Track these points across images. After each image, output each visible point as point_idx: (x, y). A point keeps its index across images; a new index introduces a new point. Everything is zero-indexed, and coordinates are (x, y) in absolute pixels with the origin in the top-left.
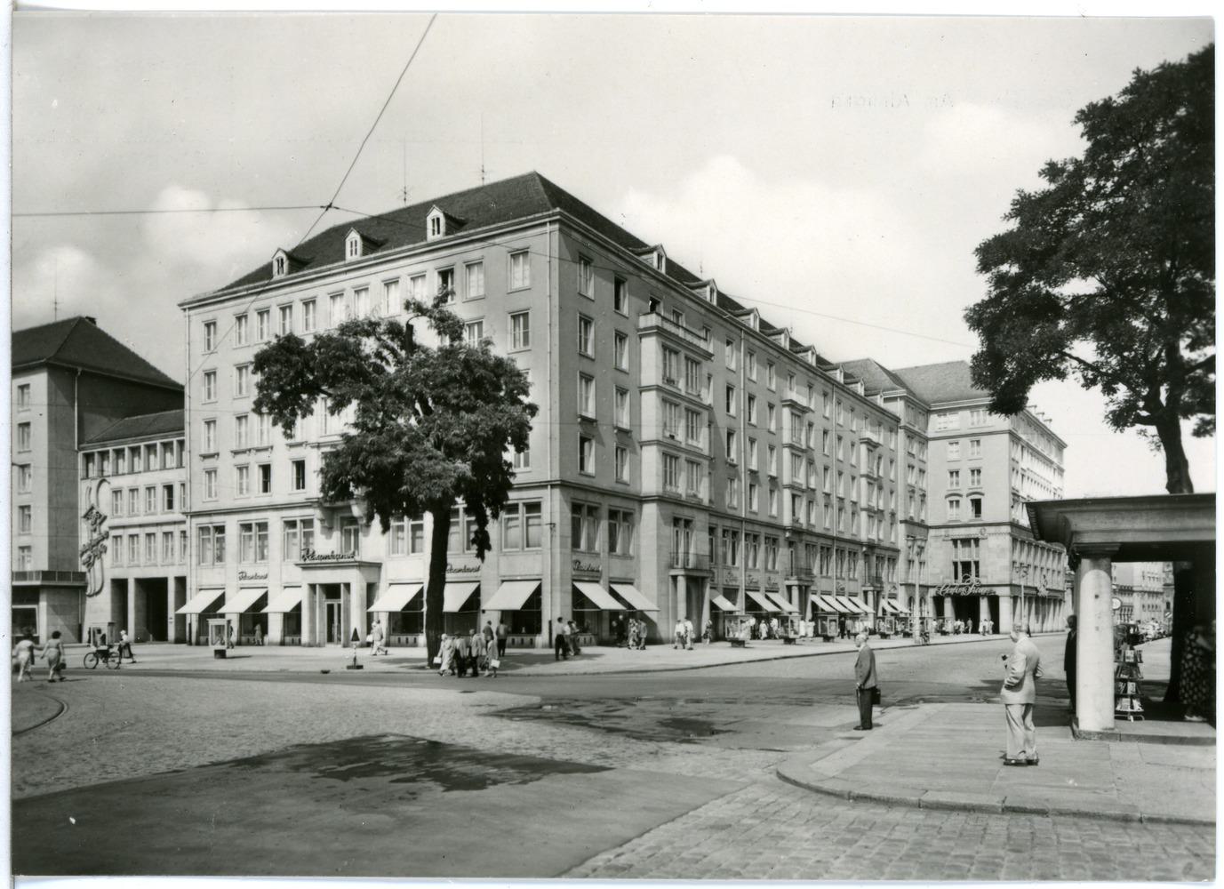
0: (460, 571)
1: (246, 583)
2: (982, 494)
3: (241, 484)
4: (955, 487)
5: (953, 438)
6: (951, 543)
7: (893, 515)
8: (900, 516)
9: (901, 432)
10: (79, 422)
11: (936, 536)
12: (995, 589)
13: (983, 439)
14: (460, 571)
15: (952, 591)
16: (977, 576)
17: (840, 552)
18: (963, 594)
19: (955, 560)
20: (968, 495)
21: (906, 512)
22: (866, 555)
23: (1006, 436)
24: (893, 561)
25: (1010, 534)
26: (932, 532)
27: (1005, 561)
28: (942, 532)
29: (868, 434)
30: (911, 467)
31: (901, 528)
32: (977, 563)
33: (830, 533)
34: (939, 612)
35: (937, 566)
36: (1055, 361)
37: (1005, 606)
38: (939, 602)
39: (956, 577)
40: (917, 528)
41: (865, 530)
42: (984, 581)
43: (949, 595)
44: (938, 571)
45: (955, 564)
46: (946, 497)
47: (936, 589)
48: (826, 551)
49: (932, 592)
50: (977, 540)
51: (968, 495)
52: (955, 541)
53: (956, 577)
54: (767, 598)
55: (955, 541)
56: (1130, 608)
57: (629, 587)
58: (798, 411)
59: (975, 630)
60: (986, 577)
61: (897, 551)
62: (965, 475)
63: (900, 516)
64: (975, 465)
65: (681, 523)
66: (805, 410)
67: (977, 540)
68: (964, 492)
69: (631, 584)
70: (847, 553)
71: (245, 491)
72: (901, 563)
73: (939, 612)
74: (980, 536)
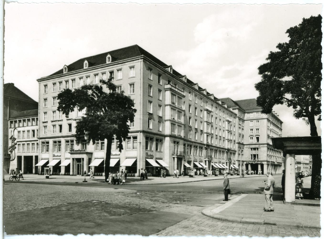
0: (114, 155)
1: (55, 157)
2: (259, 136)
5: (251, 120)
7: (235, 141)
8: (237, 142)
9: (237, 118)
12: (262, 162)
13: (260, 120)
14: (114, 155)
15: (251, 162)
16: (258, 158)
17: (220, 151)
18: (254, 163)
19: (251, 154)
21: (238, 140)
22: (227, 152)
23: (266, 120)
25: (267, 147)
26: (245, 146)
28: (248, 146)
29: (228, 119)
30: (240, 128)
31: (237, 145)
32: (258, 155)
35: (247, 155)
37: (265, 167)
38: (247, 166)
39: (252, 159)
41: (227, 145)
42: (259, 160)
45: (252, 155)
49: (245, 163)
50: (258, 149)
52: (252, 149)
53: (252, 159)
54: (199, 164)
55: (252, 149)
56: (300, 168)
59: (257, 174)
60: (260, 159)
61: (236, 151)
62: (255, 130)
63: (237, 142)
64: (257, 128)
65: (176, 143)
67: (258, 149)
68: (254, 135)
69: (162, 159)
74: (259, 147)
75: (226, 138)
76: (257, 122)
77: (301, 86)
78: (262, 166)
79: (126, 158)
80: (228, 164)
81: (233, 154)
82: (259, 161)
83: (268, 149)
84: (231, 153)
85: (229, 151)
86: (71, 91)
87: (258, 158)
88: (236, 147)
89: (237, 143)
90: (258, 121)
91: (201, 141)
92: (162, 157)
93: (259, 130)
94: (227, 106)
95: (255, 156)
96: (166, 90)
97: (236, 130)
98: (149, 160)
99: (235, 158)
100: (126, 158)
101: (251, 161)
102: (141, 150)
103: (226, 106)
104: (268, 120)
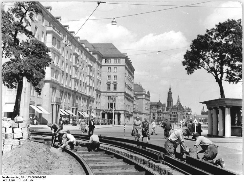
2: (117, 83)
3: (177, 117)
4: (109, 80)
6: (107, 97)
7: (94, 88)
8: (95, 89)
9: (96, 63)
10: (115, 142)
11: (103, 95)
13: (118, 67)
15: (107, 111)
17: (66, 94)
19: (109, 102)
20: (113, 83)
21: (97, 87)
22: (73, 95)
23: (124, 67)
24: (93, 102)
25: (124, 96)
26: (102, 94)
27: (122, 103)
28: (105, 94)
29: (89, 63)
30: (98, 74)
31: (95, 92)
33: (81, 93)
34: (103, 117)
35: (103, 103)
36: (228, 30)
37: (122, 117)
38: (103, 115)
40: (99, 92)
41: (88, 93)
42: (116, 109)
43: (106, 112)
44: (103, 105)
46: (107, 83)
47: (103, 111)
48: (80, 98)
49: (102, 112)
51: (113, 83)
52: (109, 97)
53: (109, 107)
54: (64, 110)
57: (40, 107)
58: (77, 56)
60: (117, 108)
61: (94, 99)
62: (112, 77)
63: (95, 89)
64: (115, 74)
65: (54, 88)
66: (78, 56)
69: (41, 106)
70: (68, 93)
71: (109, 89)
72: (95, 103)
73: (103, 117)
75: (88, 84)
76: (115, 69)
77: (193, 53)
78: (119, 115)
79: (6, 104)
80: (89, 112)
81: (68, 94)
82: (116, 110)
83: (125, 97)
84: (77, 97)
85: (89, 99)
86: (241, 114)
87: (115, 107)
88: (94, 94)
89: (96, 90)
90: (116, 68)
91: (70, 87)
92: (41, 104)
93: (111, 76)
94: (89, 50)
95: (112, 104)
96: (48, 32)
97: (95, 76)
98: (32, 106)
99: (94, 106)
100: (6, 104)
101: (108, 110)
102: (27, 97)
103: (88, 50)
104: (126, 68)
